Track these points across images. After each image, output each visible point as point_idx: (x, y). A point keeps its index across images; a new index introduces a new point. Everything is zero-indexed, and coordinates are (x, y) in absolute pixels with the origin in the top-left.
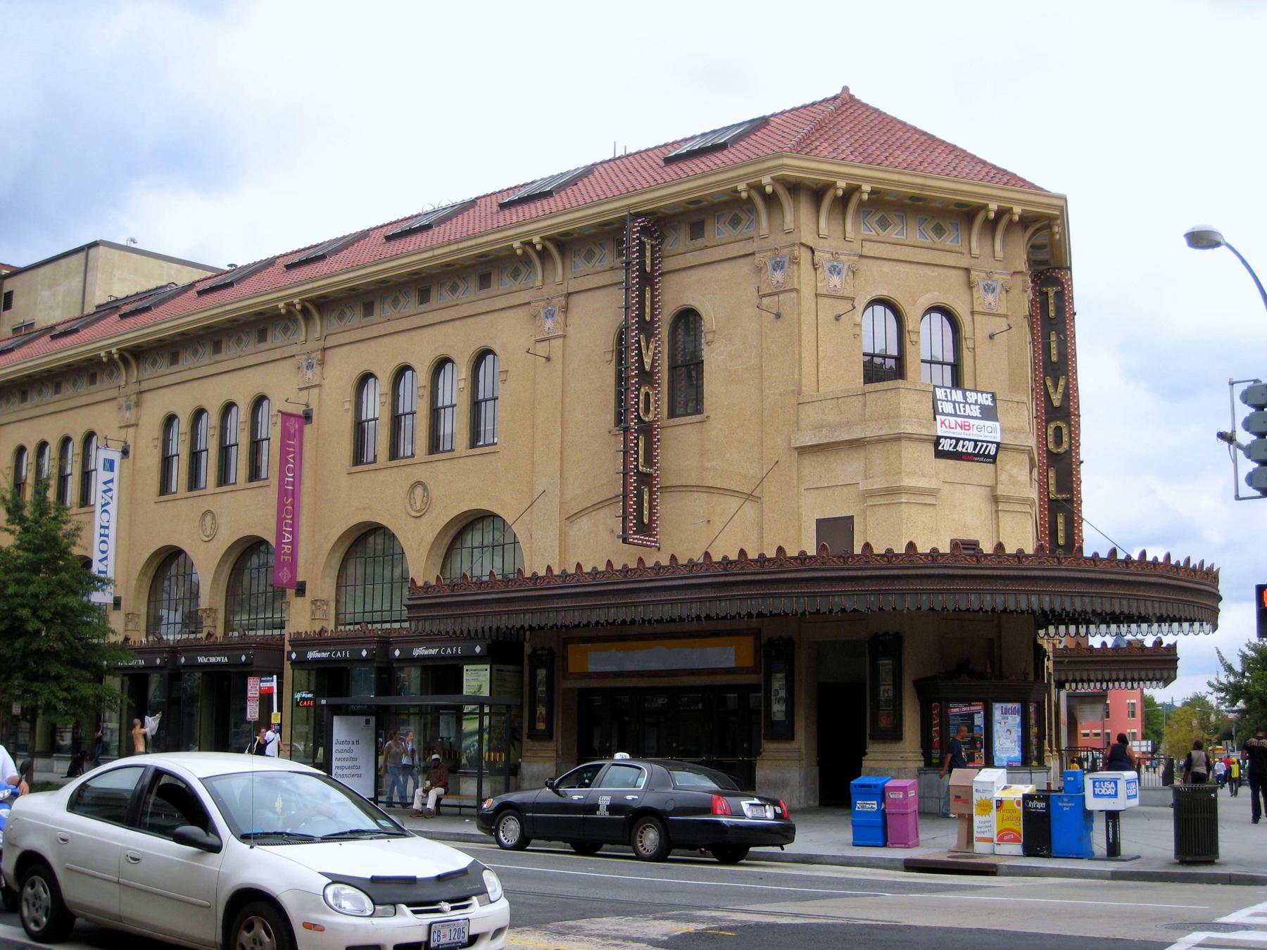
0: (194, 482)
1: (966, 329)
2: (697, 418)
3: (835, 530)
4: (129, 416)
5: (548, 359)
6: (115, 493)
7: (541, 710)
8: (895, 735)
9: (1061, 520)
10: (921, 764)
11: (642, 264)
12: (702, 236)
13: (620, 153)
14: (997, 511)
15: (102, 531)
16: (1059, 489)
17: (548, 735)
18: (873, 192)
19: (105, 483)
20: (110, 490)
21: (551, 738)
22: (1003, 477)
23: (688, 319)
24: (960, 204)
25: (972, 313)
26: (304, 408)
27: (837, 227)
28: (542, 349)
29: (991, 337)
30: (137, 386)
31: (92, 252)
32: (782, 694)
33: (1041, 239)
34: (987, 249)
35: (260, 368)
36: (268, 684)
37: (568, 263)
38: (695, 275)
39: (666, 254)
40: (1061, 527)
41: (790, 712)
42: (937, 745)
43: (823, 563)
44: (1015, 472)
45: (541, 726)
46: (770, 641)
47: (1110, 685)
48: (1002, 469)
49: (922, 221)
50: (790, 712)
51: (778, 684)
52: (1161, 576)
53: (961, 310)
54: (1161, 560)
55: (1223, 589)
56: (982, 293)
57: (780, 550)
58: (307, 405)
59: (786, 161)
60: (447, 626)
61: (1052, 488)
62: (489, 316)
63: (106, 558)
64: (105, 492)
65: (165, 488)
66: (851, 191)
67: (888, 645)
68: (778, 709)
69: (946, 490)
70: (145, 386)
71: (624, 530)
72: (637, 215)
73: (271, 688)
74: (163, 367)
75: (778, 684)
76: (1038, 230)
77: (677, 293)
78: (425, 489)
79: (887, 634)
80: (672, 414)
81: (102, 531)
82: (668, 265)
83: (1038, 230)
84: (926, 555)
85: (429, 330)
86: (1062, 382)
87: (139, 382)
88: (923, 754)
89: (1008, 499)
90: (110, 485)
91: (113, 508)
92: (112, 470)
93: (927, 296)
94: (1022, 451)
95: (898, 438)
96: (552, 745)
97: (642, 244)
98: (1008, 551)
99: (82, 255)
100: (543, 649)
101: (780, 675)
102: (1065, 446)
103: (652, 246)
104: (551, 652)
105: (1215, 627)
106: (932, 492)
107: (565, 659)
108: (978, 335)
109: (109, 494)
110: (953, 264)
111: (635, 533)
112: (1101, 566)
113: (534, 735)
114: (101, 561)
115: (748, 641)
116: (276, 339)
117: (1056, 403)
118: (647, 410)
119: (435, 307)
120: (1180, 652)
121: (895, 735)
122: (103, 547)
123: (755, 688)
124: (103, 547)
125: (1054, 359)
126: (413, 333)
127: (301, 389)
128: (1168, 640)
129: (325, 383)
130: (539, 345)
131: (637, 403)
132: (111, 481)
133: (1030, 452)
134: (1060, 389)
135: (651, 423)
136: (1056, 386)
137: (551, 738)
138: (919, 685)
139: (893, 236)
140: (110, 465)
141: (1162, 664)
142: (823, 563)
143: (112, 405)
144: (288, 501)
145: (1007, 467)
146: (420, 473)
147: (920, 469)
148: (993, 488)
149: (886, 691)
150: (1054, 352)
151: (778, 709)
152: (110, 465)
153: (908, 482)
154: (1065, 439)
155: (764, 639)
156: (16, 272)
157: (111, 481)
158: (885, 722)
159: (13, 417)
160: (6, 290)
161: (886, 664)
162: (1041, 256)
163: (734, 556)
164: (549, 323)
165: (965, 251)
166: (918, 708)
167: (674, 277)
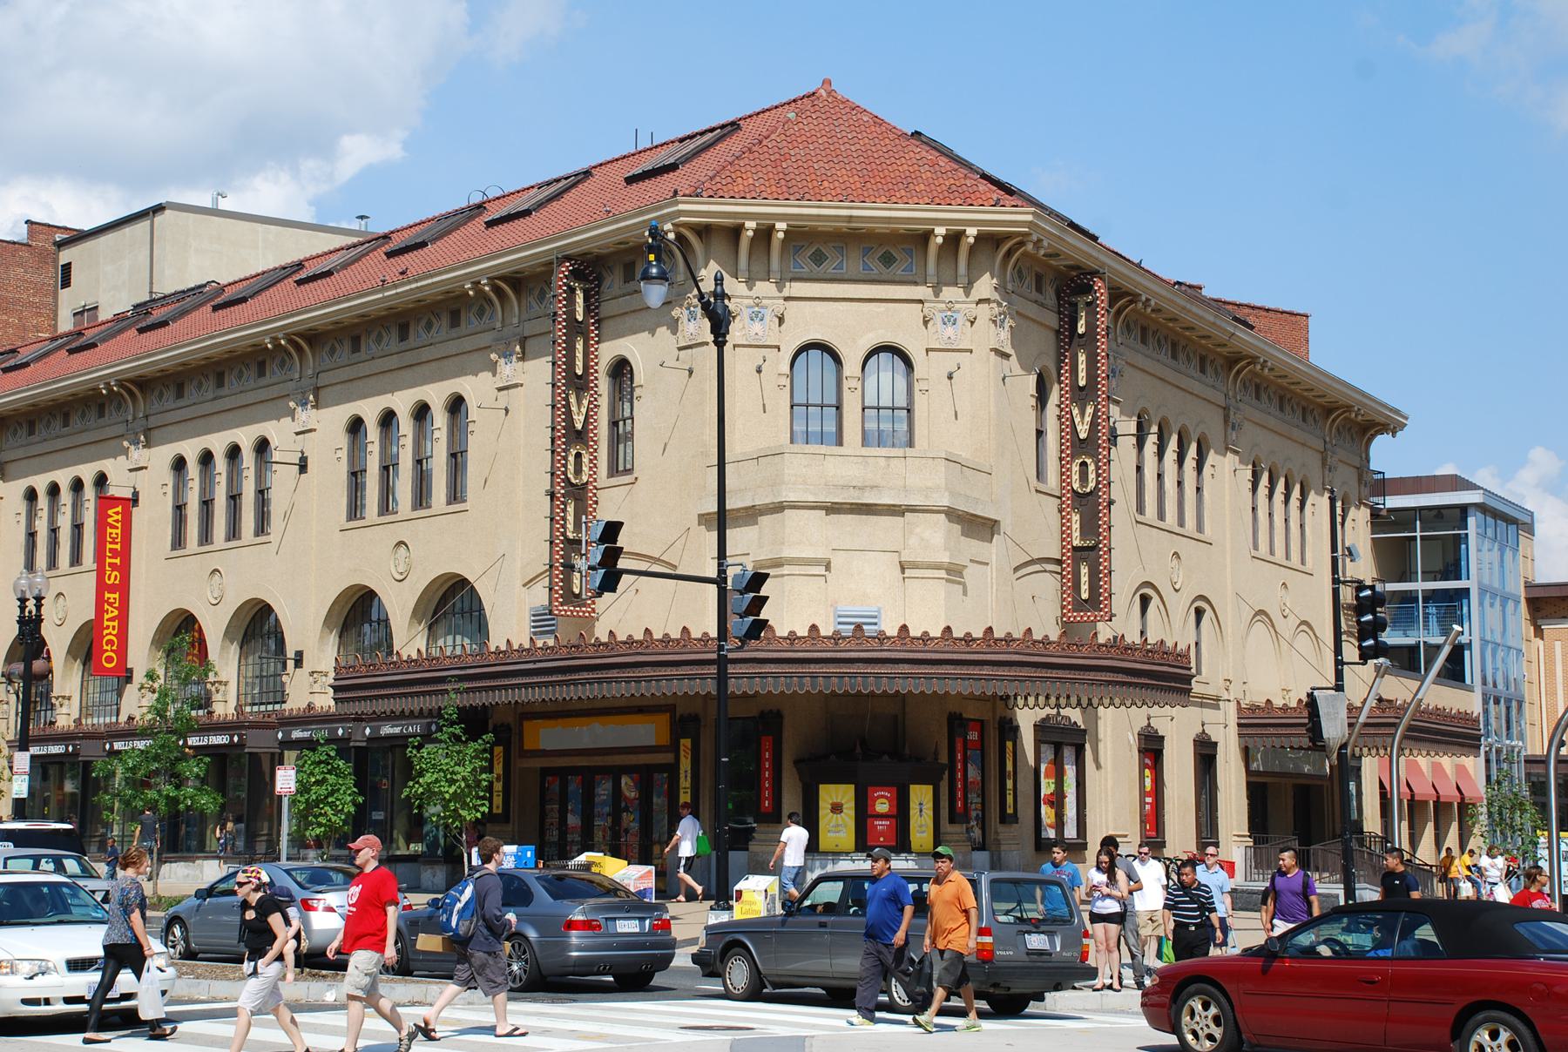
0: (206, 537)
9: (1084, 570)
11: (571, 313)
13: (644, 143)
16: (1084, 534)
21: (507, 821)
31: (158, 219)
37: (524, 302)
40: (1084, 579)
47: (1365, 750)
49: (867, 252)
59: (681, 207)
60: (415, 704)
61: (1076, 534)
65: (178, 541)
66: (765, 234)
72: (568, 258)
74: (169, 401)
86: (1089, 410)
93: (871, 335)
95: (779, 508)
96: (509, 828)
98: (823, 633)
99: (142, 227)
112: (931, 645)
115: (664, 719)
116: (274, 373)
117: (1083, 435)
118: (578, 471)
119: (413, 345)
123: (661, 768)
125: (1082, 383)
127: (297, 434)
131: (565, 466)
134: (1088, 419)
136: (1082, 414)
137: (507, 821)
138: (797, 762)
144: (114, 586)
145: (918, 530)
146: (402, 532)
147: (803, 535)
153: (787, 553)
154: (1092, 476)
156: (79, 237)
160: (62, 262)
163: (639, 636)
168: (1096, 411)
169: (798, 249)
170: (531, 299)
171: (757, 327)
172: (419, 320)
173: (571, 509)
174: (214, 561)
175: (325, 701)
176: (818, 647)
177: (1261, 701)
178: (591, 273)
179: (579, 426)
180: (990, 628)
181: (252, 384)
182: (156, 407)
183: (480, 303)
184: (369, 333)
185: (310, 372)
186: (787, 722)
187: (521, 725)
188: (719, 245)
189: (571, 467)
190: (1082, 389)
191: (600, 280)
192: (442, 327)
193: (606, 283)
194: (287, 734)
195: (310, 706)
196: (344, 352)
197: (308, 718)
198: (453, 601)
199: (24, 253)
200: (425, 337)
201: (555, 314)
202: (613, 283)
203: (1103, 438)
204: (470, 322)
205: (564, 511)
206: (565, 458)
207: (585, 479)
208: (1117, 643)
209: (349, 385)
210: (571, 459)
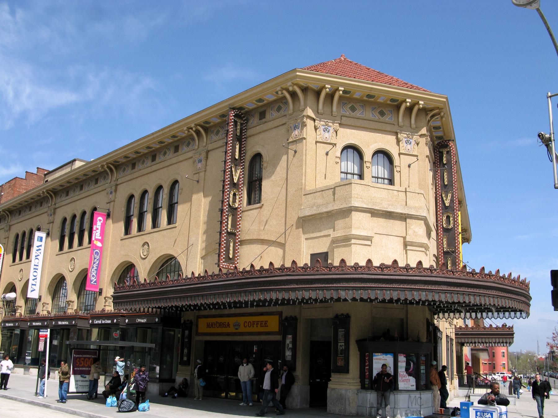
1: (396, 162)
2: (258, 205)
3: (320, 258)
4: (51, 218)
5: (198, 182)
6: (42, 251)
7: (186, 351)
8: (345, 370)
10: (359, 387)
12: (264, 118)
14: (406, 251)
15: (35, 267)
16: (449, 245)
17: (188, 363)
18: (345, 92)
19: (38, 247)
20: (40, 250)
22: (410, 232)
23: (258, 156)
24: (393, 100)
25: (400, 154)
26: (107, 211)
27: (327, 110)
28: (196, 177)
29: (409, 166)
30: (54, 206)
32: (291, 346)
33: (436, 122)
34: (407, 123)
35: (95, 195)
36: (45, 333)
37: (209, 137)
38: (261, 136)
39: (248, 127)
41: (294, 356)
42: (367, 376)
43: (294, 271)
44: (416, 229)
45: (185, 359)
46: (286, 318)
48: (409, 228)
49: (373, 109)
50: (294, 356)
51: (289, 339)
52: (494, 282)
53: (394, 151)
54: (494, 273)
55: (532, 293)
56: (405, 144)
57: (271, 264)
58: (109, 210)
62: (177, 164)
63: (36, 279)
64: (37, 250)
67: (342, 321)
68: (288, 353)
69: (376, 239)
70: (57, 206)
71: (219, 261)
72: (234, 109)
73: (47, 335)
75: (289, 339)
76: (433, 116)
77: (254, 146)
78: (148, 246)
79: (342, 314)
80: (249, 203)
81: (35, 267)
82: (250, 132)
83: (433, 116)
84: (352, 267)
85: (155, 173)
86: (450, 195)
87: (55, 204)
88: (361, 382)
89: (412, 244)
90: (40, 248)
91: (41, 257)
92: (41, 241)
94: (421, 219)
97: (236, 122)
100: (188, 320)
101: (290, 336)
102: (451, 226)
103: (241, 124)
104: (191, 322)
105: (528, 314)
106: (369, 239)
107: (197, 325)
108: (402, 165)
109: (40, 251)
110: (389, 130)
111: (224, 262)
113: (183, 363)
114: (33, 280)
117: (447, 205)
118: (234, 201)
120: (515, 330)
121: (345, 370)
122: (35, 274)
124: (35, 274)
125: (446, 183)
126: (148, 175)
127: (107, 203)
128: (509, 322)
129: (116, 200)
130: (195, 175)
131: (229, 198)
132: (41, 246)
133: (425, 220)
134: (449, 198)
135: (236, 209)
136: (447, 196)
138: (359, 342)
139: (358, 115)
140: (41, 239)
141: (506, 335)
142: (294, 271)
143: (46, 214)
145: (412, 227)
147: (361, 224)
148: (404, 238)
149: (341, 345)
150: (446, 180)
151: (288, 353)
152: (41, 239)
153: (354, 232)
155: (284, 318)
157: (41, 246)
158: (340, 363)
159: (15, 222)
161: (341, 332)
162: (440, 134)
164: (200, 165)
165: (396, 123)
166: (358, 356)
167: (252, 138)
168: (452, 197)
169: (344, 104)
170: (212, 135)
171: (327, 135)
172: (160, 152)
173: (230, 219)
174: (72, 255)
175: (110, 308)
176: (398, 273)
177: (363, 263)
178: (244, 117)
179: (235, 181)
180: (498, 270)
181: (93, 187)
182: (59, 200)
183: (188, 140)
184: (139, 161)
185: (114, 179)
186: (353, 319)
187: (197, 320)
188: (311, 98)
189: (231, 199)
190: (446, 185)
191: (247, 120)
192: (170, 154)
193: (251, 121)
194: (93, 322)
195: (103, 310)
196: (129, 170)
197: (103, 315)
198: (168, 264)
199: (35, 177)
200: (162, 158)
201: (228, 131)
202: (254, 120)
203: (456, 205)
204: (184, 149)
205: (227, 218)
206: (229, 194)
207: (237, 206)
208: (16, 351)
209: (129, 182)
210: (231, 196)
